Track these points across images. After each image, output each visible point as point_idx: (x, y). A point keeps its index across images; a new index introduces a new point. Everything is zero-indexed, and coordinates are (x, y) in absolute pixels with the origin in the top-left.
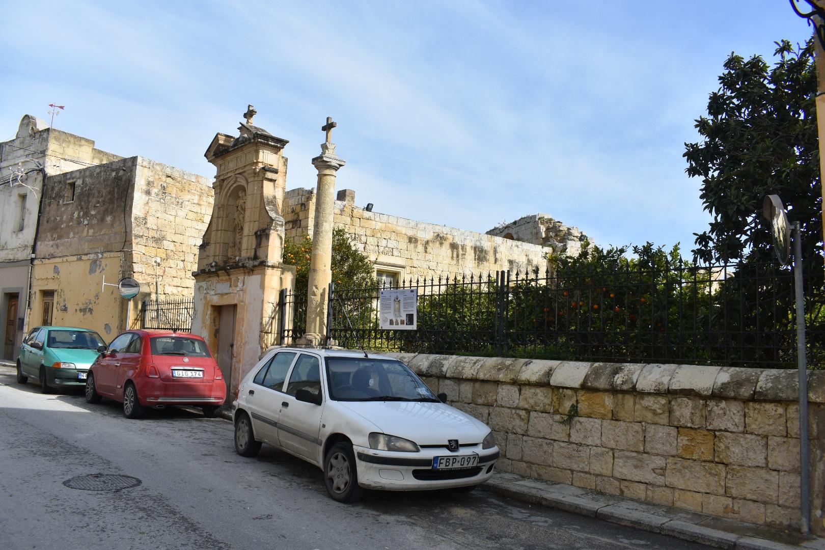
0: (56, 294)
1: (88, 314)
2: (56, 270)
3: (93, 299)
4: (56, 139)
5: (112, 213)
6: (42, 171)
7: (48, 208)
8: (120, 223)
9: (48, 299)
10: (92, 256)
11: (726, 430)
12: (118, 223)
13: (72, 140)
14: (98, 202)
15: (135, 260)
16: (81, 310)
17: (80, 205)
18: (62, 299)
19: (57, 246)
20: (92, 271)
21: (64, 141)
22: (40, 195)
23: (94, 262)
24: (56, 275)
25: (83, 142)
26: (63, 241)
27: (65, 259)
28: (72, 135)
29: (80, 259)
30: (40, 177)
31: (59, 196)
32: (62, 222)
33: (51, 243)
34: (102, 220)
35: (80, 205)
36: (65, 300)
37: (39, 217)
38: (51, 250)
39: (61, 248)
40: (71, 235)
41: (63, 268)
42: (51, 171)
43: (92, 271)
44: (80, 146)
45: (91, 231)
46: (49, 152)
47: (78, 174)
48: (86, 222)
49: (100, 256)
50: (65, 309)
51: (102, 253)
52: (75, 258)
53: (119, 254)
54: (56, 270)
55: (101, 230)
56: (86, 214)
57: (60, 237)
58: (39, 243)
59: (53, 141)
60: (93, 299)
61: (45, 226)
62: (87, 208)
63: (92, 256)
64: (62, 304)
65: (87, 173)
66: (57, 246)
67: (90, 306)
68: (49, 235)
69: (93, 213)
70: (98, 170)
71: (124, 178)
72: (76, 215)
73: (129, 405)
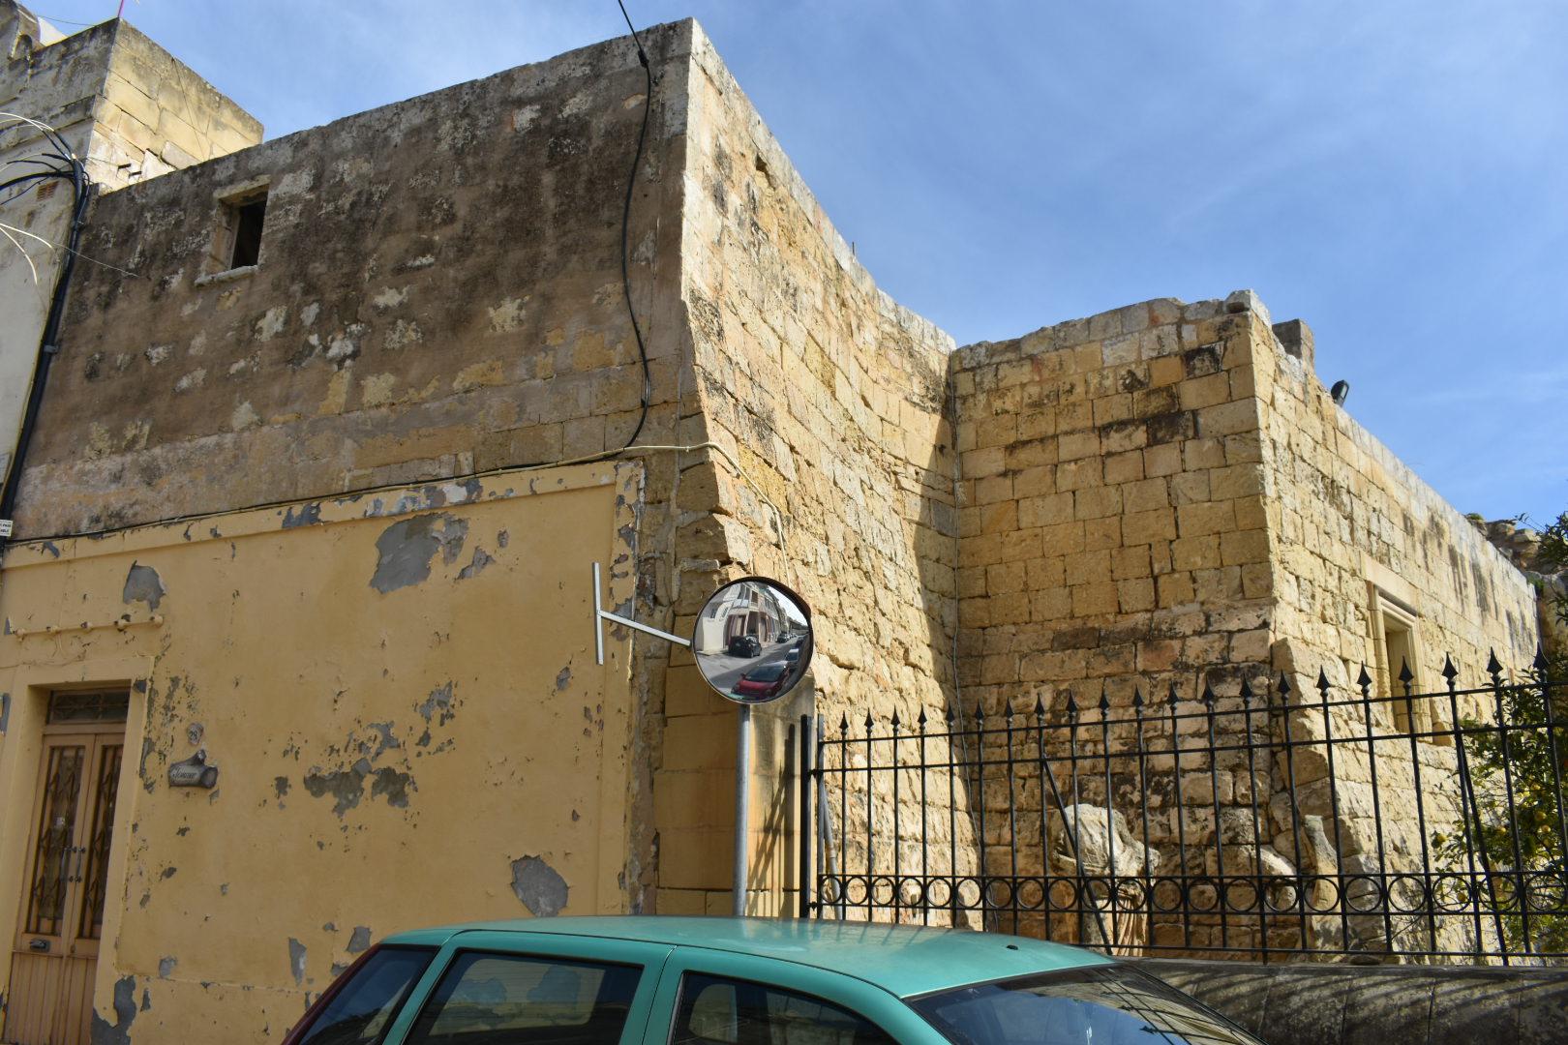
0: (137, 706)
1: (373, 807)
2: (143, 585)
3: (407, 724)
4: (142, 70)
5: (521, 284)
6: (73, 174)
7: (95, 319)
8: (595, 320)
9: (83, 734)
10: (392, 501)
11: (915, 404)
12: (575, 325)
13: (193, 91)
14: (426, 248)
15: (725, 501)
16: (315, 783)
17: (301, 274)
18: (178, 729)
19: (150, 475)
20: (386, 577)
21: (164, 86)
22: (53, 275)
23: (415, 527)
24: (139, 612)
25: (227, 116)
26: (184, 447)
27: (200, 530)
28: (193, 76)
29: (311, 520)
30: (62, 199)
31: (164, 257)
32: (180, 363)
33: (111, 464)
34: (460, 321)
35: (301, 274)
36: (195, 733)
37: (43, 360)
38: (114, 497)
39: (167, 485)
40: (243, 414)
41: (190, 578)
42: (106, 175)
43: (386, 577)
44: (218, 125)
45: (378, 387)
46: (106, 111)
47: (285, 155)
48: (339, 347)
49: (454, 493)
50: (203, 778)
51: (471, 483)
52: (272, 519)
53: (604, 473)
54: (143, 585)
55: (452, 370)
56: (344, 310)
57: (165, 433)
58: (34, 473)
59: (128, 72)
60: (407, 724)
61: (71, 374)
62: (351, 281)
63: (392, 501)
64: (181, 752)
65: (346, 141)
66: (150, 475)
67: (389, 759)
68: (98, 430)
69: (389, 298)
70: (416, 118)
71: (600, 124)
72: (272, 322)
73: (48, 348)
